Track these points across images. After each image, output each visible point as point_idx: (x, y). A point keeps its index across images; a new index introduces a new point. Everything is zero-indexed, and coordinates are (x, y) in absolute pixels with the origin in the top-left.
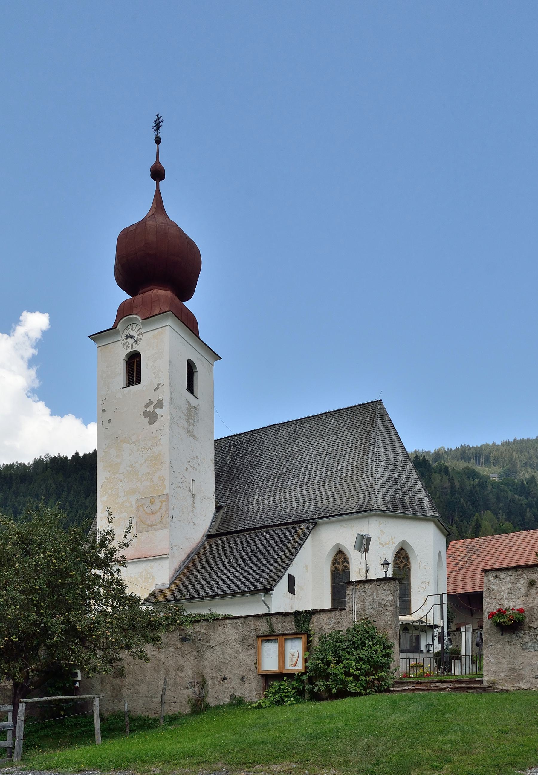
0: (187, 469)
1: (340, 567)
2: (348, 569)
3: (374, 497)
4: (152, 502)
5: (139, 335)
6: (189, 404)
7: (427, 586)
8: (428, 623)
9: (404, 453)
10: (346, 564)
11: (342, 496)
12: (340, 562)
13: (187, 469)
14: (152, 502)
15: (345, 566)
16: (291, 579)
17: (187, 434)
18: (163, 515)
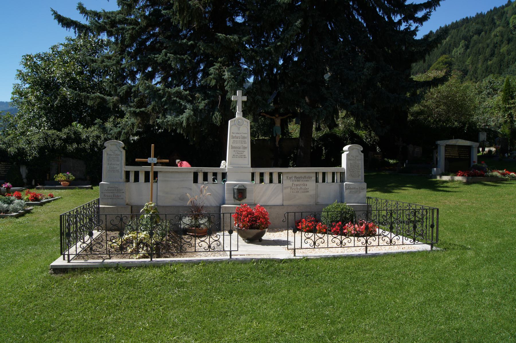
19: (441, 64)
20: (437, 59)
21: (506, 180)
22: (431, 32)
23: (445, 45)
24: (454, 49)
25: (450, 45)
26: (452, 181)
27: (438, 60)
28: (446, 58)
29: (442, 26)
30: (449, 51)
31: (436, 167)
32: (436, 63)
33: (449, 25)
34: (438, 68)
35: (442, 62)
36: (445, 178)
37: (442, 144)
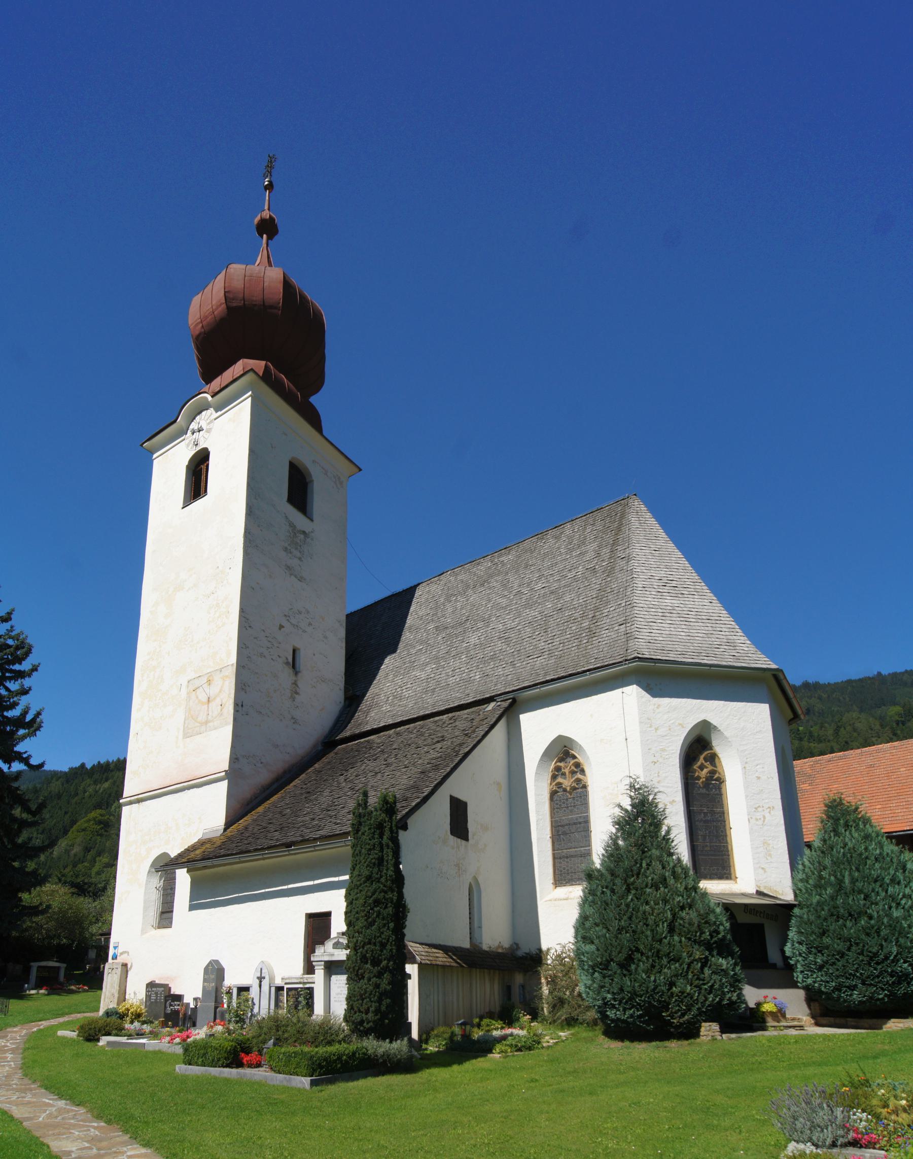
0: (283, 627)
1: (567, 783)
2: (585, 787)
3: (633, 637)
4: (209, 682)
5: (209, 424)
6: (292, 525)
7: (767, 815)
8: (780, 899)
9: (687, 568)
10: (579, 776)
11: (565, 648)
12: (567, 773)
13: (281, 627)
14: (209, 682)
15: (578, 781)
16: (459, 810)
17: (286, 571)
18: (224, 701)
19: (92, 822)
20: (86, 813)
21: (79, 992)
22: (83, 765)
23: (102, 793)
24: (114, 802)
25: (110, 795)
26: (38, 993)
27: (89, 815)
28: (101, 815)
29: (102, 762)
30: (107, 804)
31: (28, 983)
32: (85, 819)
33: (113, 761)
34: (86, 828)
35: (94, 819)
36: (33, 992)
37: (35, 965)
